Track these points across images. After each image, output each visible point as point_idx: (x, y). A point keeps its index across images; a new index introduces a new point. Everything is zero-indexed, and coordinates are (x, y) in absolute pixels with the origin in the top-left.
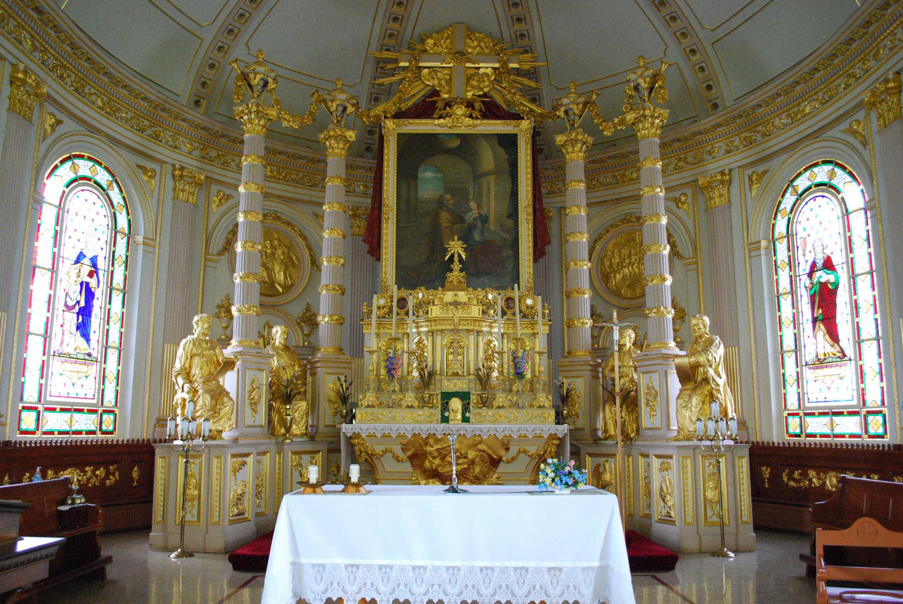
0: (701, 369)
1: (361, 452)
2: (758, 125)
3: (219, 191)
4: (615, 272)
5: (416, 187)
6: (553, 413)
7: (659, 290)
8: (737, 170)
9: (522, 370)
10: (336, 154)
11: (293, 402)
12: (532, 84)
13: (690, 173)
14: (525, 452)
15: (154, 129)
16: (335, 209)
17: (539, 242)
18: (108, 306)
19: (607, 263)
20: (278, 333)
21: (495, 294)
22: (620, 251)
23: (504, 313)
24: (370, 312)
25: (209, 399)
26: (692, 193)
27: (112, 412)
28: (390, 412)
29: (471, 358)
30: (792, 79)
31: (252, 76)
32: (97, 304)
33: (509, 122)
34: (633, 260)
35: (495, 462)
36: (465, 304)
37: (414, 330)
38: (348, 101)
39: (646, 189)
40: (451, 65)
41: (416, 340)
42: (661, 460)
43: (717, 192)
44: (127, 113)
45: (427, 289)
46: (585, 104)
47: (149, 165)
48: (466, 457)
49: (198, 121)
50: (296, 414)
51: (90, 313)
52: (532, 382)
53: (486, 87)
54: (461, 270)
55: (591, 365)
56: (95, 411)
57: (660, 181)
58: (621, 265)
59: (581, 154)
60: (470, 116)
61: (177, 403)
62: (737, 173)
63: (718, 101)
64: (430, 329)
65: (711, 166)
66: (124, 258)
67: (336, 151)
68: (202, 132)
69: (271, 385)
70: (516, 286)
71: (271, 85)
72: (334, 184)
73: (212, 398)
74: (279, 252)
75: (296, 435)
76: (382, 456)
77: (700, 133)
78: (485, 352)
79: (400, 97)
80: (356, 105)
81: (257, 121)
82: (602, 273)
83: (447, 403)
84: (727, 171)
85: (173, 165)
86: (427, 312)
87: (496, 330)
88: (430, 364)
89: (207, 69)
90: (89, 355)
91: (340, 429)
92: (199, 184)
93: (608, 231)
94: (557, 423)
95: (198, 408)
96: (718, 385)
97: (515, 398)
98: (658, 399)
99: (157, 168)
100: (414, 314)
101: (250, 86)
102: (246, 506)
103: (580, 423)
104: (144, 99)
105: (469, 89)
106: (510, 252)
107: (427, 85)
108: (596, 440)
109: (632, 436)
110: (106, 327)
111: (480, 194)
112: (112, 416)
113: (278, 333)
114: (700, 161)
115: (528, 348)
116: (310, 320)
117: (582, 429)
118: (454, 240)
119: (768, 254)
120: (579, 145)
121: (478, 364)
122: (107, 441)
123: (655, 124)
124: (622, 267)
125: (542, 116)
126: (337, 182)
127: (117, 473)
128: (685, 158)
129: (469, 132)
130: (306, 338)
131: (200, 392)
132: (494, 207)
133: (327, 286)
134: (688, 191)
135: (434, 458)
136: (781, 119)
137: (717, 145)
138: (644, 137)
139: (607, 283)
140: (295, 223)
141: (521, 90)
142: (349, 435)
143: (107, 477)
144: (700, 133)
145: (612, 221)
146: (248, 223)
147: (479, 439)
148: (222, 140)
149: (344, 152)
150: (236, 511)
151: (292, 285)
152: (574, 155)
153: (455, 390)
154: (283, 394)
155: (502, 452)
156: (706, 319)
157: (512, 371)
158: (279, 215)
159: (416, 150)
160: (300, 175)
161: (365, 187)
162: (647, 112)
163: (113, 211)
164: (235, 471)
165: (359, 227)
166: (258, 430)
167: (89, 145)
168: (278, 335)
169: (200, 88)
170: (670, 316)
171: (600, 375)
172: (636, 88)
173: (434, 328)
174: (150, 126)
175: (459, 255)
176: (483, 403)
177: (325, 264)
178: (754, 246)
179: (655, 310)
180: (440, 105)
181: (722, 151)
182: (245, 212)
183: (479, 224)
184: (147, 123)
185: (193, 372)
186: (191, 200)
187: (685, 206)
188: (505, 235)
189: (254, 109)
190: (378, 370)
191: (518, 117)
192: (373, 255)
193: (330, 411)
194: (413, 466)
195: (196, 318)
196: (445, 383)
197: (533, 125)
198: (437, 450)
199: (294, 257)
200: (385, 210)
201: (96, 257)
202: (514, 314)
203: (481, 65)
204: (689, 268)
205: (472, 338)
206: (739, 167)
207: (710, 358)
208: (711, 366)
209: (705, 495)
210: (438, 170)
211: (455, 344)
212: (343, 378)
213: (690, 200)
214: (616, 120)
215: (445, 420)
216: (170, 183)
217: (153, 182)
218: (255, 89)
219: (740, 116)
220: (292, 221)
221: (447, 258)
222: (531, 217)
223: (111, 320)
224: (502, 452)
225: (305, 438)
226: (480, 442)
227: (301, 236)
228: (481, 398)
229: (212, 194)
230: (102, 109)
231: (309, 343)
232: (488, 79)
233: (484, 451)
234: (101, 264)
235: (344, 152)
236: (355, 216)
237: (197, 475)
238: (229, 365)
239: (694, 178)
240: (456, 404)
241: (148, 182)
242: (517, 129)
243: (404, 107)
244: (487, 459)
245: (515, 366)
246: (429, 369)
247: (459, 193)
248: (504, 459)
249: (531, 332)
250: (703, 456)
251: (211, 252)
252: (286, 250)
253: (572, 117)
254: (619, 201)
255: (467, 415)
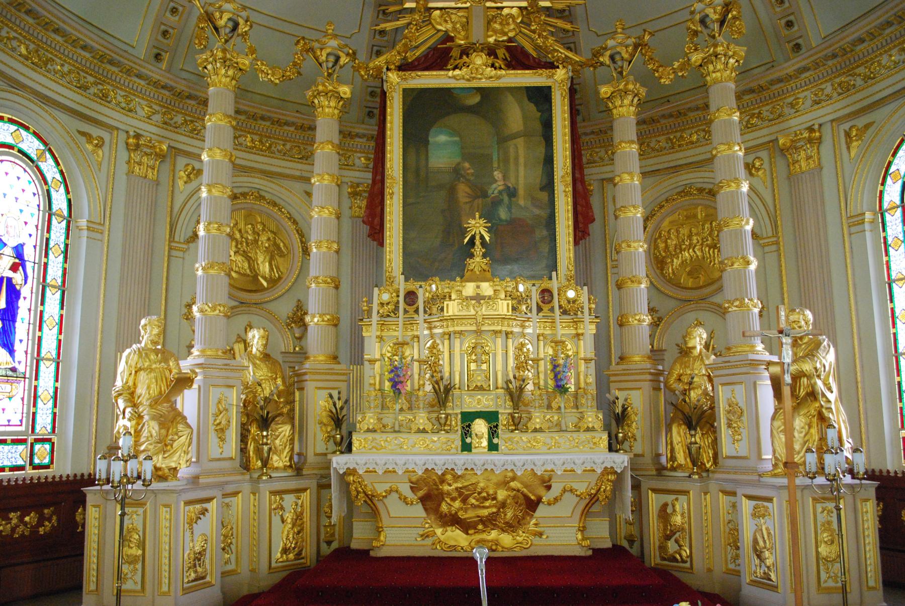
0: (805, 380)
1: (358, 492)
2: (858, 67)
3: (188, 165)
4: (672, 257)
5: (427, 151)
6: (605, 437)
7: (742, 276)
8: (829, 124)
9: (562, 383)
10: (327, 115)
11: (273, 426)
12: (568, 27)
13: (765, 131)
14: (571, 491)
15: (100, 87)
16: (326, 182)
17: (580, 218)
18: (40, 308)
19: (662, 245)
20: (255, 337)
21: (529, 284)
22: (678, 231)
23: (540, 309)
24: (369, 312)
25: (157, 428)
26: (775, 155)
27: (49, 440)
28: (396, 438)
29: (499, 367)
30: (856, 35)
31: (217, 15)
32: (23, 306)
33: (540, 71)
34: (695, 241)
35: (532, 505)
36: (490, 298)
37: (426, 332)
38: (340, 48)
39: (722, 147)
40: (468, 5)
41: (428, 345)
42: (754, 503)
43: (803, 153)
44: (62, 65)
45: (441, 280)
46: (636, 46)
47: (95, 131)
48: (494, 499)
49: (156, 77)
50: (277, 442)
51: (13, 319)
52: (576, 396)
53: (510, 31)
54: (484, 256)
55: (651, 374)
56: (24, 441)
57: (738, 138)
58: (679, 248)
59: (632, 109)
60: (493, 66)
61: (118, 432)
62: (829, 131)
63: (800, 41)
64: (446, 330)
65: (793, 122)
66: (62, 246)
67: (327, 110)
68: (163, 91)
69: (246, 404)
70: (554, 274)
71: (243, 28)
72: (325, 151)
73: (162, 425)
74: (263, 238)
75: (277, 468)
76: (386, 497)
77: (780, 80)
78: (517, 358)
79: (405, 45)
80: (353, 56)
81: (223, 71)
82: (656, 258)
83: (469, 426)
84: (816, 127)
85: (127, 132)
86: (442, 309)
87: (529, 331)
88: (447, 375)
89: (168, 14)
90: (14, 370)
91: (329, 462)
92: (162, 157)
93: (661, 207)
94: (611, 449)
95: (142, 440)
96: (829, 401)
97: (556, 418)
98: (744, 418)
99: (106, 136)
100: (425, 312)
101: (216, 29)
102: (208, 567)
103: (638, 448)
104: (84, 48)
105: (490, 33)
106: (545, 233)
107: (439, 31)
108: (660, 470)
109: (708, 466)
110: (38, 334)
111: (506, 161)
112: (48, 446)
113: (255, 337)
114: (780, 116)
115: (570, 353)
116: (298, 319)
117: (642, 456)
118: (474, 218)
119: (874, 230)
120: (630, 97)
121: (507, 375)
122: (46, 478)
123: (730, 65)
124: (681, 250)
125: (582, 65)
126: (328, 148)
127: (54, 518)
128: (760, 113)
129: (491, 85)
130: (297, 342)
131: (146, 418)
132: (524, 176)
133: (317, 278)
134: (764, 154)
135: (453, 499)
136: (891, 56)
137: (802, 95)
138: (716, 82)
139: (662, 269)
140: (282, 203)
141: (552, 34)
142: (341, 472)
143: (40, 523)
144: (780, 80)
145: (667, 195)
146: (211, 197)
147: (510, 474)
148: (189, 101)
149: (336, 112)
150: (193, 575)
151: (280, 278)
152: (623, 110)
153: (479, 408)
154: (259, 416)
155: (541, 491)
156: (809, 314)
157: (551, 383)
158: (263, 193)
159: (425, 110)
160: (288, 146)
161: (367, 159)
162: (720, 49)
163: (45, 188)
164: (192, 522)
165: (361, 208)
166: (226, 465)
167: (8, 103)
168: (256, 341)
169: (160, 38)
170: (756, 310)
171: (662, 385)
172: (703, 21)
173: (451, 329)
174: (96, 84)
175: (482, 237)
176: (514, 425)
177: (315, 250)
178: (857, 221)
179: (737, 303)
180: (455, 53)
181: (809, 102)
182: (208, 185)
183: (506, 199)
184: (91, 79)
185: (139, 391)
186: (150, 175)
187: (760, 173)
188: (537, 211)
189: (220, 54)
190: (381, 382)
191: (552, 66)
192: (374, 240)
193: (321, 436)
194: (426, 509)
195: (143, 322)
196: (467, 399)
197: (571, 74)
198: (457, 489)
199: (282, 245)
200: (388, 182)
201: (22, 245)
202: (552, 310)
203: (505, 4)
204: (767, 249)
205: (499, 341)
206: (832, 121)
207: (818, 366)
208: (819, 376)
209: (817, 552)
210: (454, 132)
211: (479, 350)
212: (335, 394)
213: (766, 166)
214: (676, 65)
215: (467, 448)
216: (123, 155)
217: (100, 152)
218: (222, 32)
219: (834, 56)
220: (278, 201)
221: (466, 240)
222: (570, 189)
223: (44, 325)
224: (541, 491)
225: (290, 472)
226: (513, 479)
227: (290, 219)
228: (513, 418)
229: (177, 169)
230: (27, 58)
231: (302, 348)
232: (514, 21)
233: (518, 491)
234: (29, 254)
235: (336, 112)
236: (354, 194)
237: (140, 528)
238: (184, 382)
239: (773, 138)
240: (480, 427)
241: (94, 152)
242: (551, 80)
243: (411, 56)
244: (521, 500)
245: (556, 376)
246: (446, 382)
247: (482, 161)
248: (544, 499)
249: (574, 332)
250: (814, 499)
251: (177, 239)
252: (271, 235)
253: (620, 63)
254: (675, 169)
255: (495, 441)
